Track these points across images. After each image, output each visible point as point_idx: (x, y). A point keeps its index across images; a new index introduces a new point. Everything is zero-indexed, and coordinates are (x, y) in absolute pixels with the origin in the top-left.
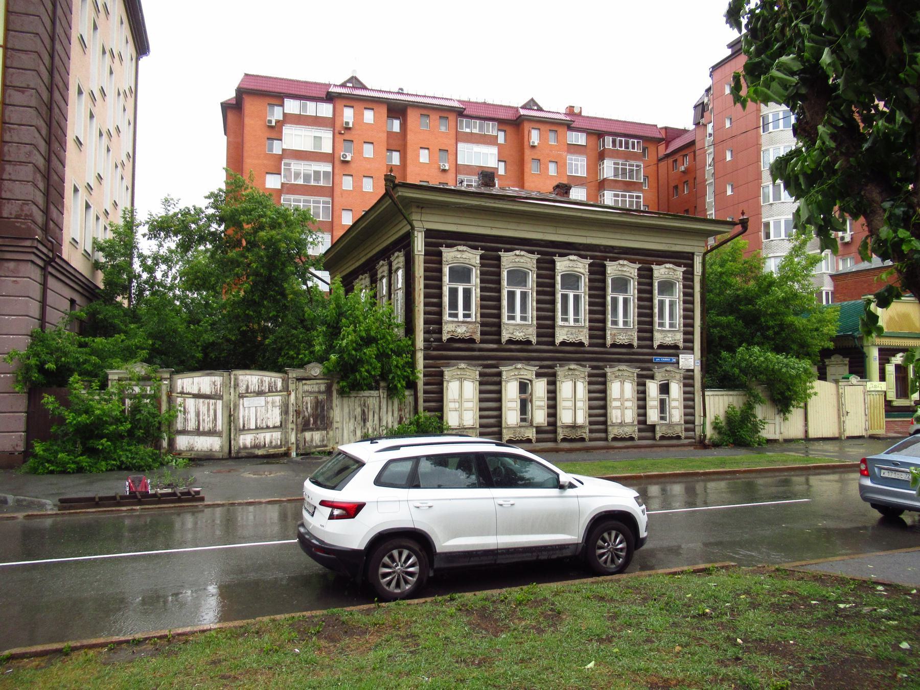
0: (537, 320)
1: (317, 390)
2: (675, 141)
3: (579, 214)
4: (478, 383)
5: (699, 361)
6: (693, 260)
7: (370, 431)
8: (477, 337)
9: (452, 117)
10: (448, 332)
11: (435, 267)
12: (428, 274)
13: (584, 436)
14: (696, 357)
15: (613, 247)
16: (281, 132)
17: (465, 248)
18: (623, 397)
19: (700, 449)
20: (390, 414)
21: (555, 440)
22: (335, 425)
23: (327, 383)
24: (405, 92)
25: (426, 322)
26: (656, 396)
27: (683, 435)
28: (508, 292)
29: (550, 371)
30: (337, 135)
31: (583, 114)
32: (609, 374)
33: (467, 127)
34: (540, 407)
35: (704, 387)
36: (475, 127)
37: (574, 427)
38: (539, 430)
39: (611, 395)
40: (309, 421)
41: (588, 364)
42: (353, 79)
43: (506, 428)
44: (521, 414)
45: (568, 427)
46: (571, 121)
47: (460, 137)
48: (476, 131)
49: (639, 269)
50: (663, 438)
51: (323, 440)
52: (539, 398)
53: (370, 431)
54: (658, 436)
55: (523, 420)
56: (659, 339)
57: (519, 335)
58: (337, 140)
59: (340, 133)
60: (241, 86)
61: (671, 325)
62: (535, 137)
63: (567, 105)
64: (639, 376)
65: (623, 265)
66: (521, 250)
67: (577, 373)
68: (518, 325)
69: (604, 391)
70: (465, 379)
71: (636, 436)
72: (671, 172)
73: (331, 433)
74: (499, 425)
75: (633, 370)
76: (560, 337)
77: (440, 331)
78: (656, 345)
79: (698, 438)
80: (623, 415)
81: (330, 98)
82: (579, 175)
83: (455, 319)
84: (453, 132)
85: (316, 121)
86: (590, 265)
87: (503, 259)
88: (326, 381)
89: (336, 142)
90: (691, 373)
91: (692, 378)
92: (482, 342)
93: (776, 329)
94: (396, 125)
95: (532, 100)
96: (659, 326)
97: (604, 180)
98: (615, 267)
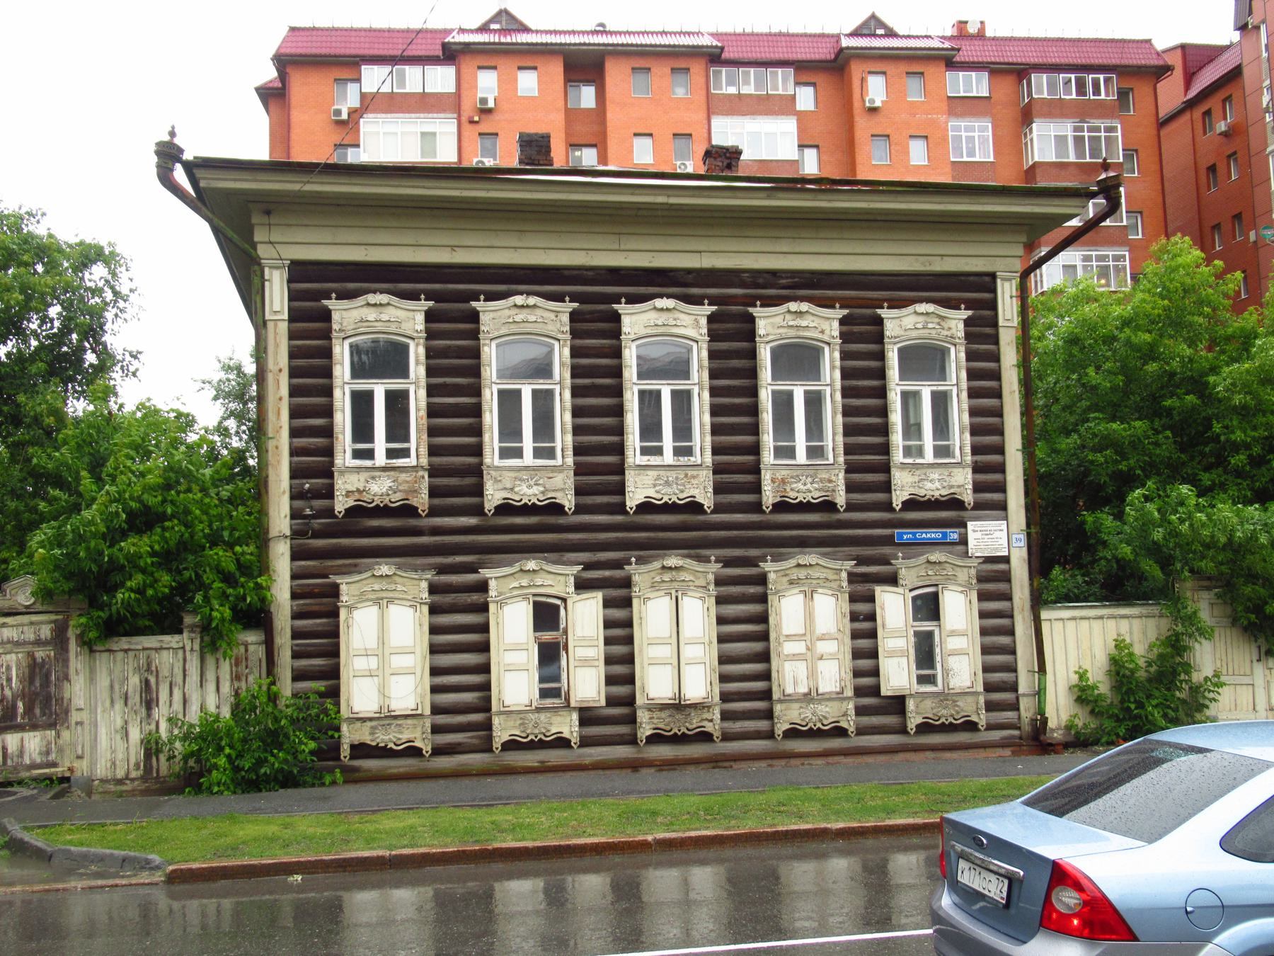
0: (575, 454)
1: (32, 637)
2: (1204, 71)
3: (661, 199)
4: (426, 609)
5: (1023, 537)
6: (994, 291)
7: (163, 726)
8: (422, 500)
9: (697, 68)
10: (348, 494)
11: (606, 366)
12: (300, 362)
13: (709, 728)
14: (1014, 528)
15: (774, 273)
16: (358, 131)
17: (384, 298)
18: (812, 632)
19: (1032, 753)
20: (211, 687)
21: (632, 740)
22: (75, 717)
23: (55, 622)
24: (607, 29)
25: (295, 473)
26: (901, 624)
27: (982, 719)
28: (502, 393)
29: (617, 573)
30: (466, 126)
31: (989, 33)
32: (772, 576)
33: (730, 82)
34: (586, 663)
35: (1038, 602)
36: (747, 82)
37: (678, 707)
38: (587, 716)
39: (778, 626)
40: (14, 707)
41: (713, 554)
42: (503, 14)
43: (500, 713)
44: (920, 665)
45: (664, 707)
46: (953, 49)
47: (714, 106)
48: (749, 89)
49: (843, 322)
50: (924, 728)
51: (48, 753)
52: (584, 638)
53: (163, 726)
54: (497, 744)
55: (544, 694)
56: (904, 485)
57: (530, 492)
58: (465, 134)
59: (472, 122)
60: (283, 51)
61: (941, 451)
62: (876, 90)
63: (954, 21)
64: (853, 577)
65: (800, 314)
66: (529, 294)
67: (684, 576)
68: (527, 468)
69: (763, 618)
70: (391, 601)
71: (850, 724)
72: (1201, 138)
73: (66, 734)
74: (485, 706)
75: (837, 565)
76: (638, 490)
77: (329, 493)
78: (898, 498)
79: (1027, 728)
80: (812, 674)
81: (450, 54)
82: (977, 159)
83: (368, 463)
84: (700, 97)
85: (424, 103)
86: (711, 319)
87: (483, 318)
88: (53, 617)
89: (464, 140)
90: (1002, 567)
91: (1006, 577)
92: (433, 512)
93: (1257, 450)
94: (587, 96)
95: (873, 17)
96: (905, 456)
97: (1035, 165)
98: (779, 320)
